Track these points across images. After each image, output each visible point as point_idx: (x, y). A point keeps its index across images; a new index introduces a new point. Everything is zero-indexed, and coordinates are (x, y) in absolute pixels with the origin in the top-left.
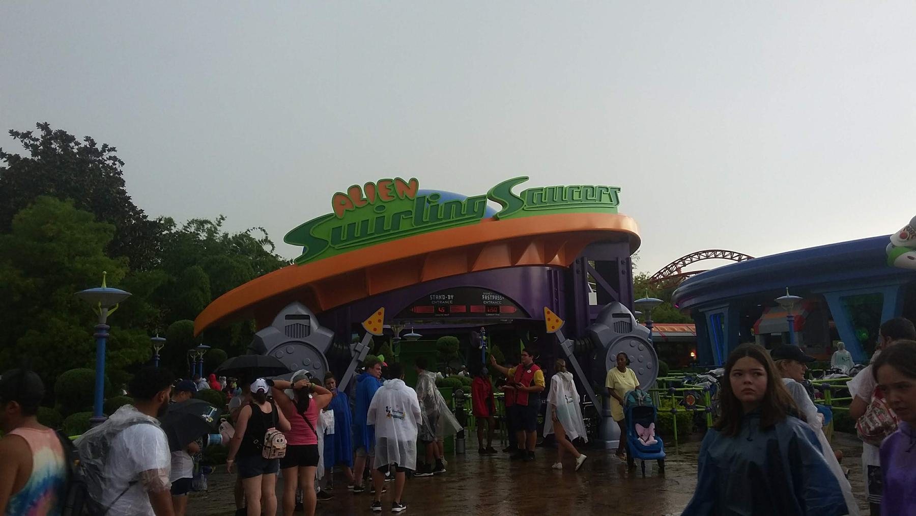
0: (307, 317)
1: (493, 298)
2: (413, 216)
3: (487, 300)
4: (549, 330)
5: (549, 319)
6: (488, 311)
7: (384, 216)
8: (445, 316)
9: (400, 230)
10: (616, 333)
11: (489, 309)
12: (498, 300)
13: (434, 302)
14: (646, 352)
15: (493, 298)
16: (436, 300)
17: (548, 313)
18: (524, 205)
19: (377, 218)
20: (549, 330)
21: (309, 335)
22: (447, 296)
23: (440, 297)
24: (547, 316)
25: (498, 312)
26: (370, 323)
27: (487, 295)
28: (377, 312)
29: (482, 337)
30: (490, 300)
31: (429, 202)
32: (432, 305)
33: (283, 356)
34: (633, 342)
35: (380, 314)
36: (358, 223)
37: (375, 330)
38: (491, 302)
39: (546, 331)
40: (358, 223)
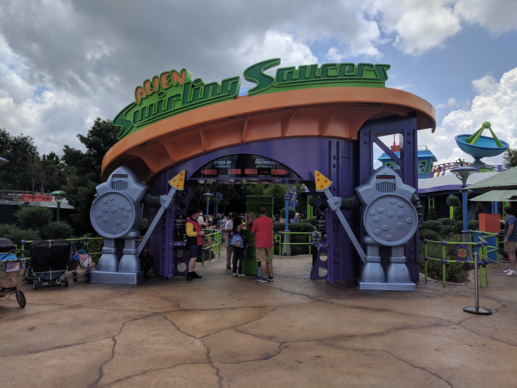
0: (126, 176)
1: (265, 163)
2: (181, 98)
3: (259, 165)
4: (171, 182)
5: (318, 180)
6: (261, 173)
7: (293, 72)
8: (225, 177)
9: (363, 77)
10: (378, 191)
11: (262, 171)
12: (269, 165)
13: (258, 166)
14: (407, 208)
15: (265, 163)
16: (218, 165)
17: (318, 175)
18: (274, 82)
19: (288, 72)
20: (171, 182)
21: (126, 189)
22: (227, 162)
23: (222, 163)
24: (316, 177)
25: (270, 174)
26: (174, 181)
27: (260, 161)
28: (180, 174)
29: (294, 192)
30: (262, 165)
31: (193, 86)
32: (256, 168)
33: (403, 227)
34: (393, 200)
35: (182, 174)
36: (148, 107)
37: (178, 186)
38: (263, 166)
39: (315, 189)
40: (148, 107)
